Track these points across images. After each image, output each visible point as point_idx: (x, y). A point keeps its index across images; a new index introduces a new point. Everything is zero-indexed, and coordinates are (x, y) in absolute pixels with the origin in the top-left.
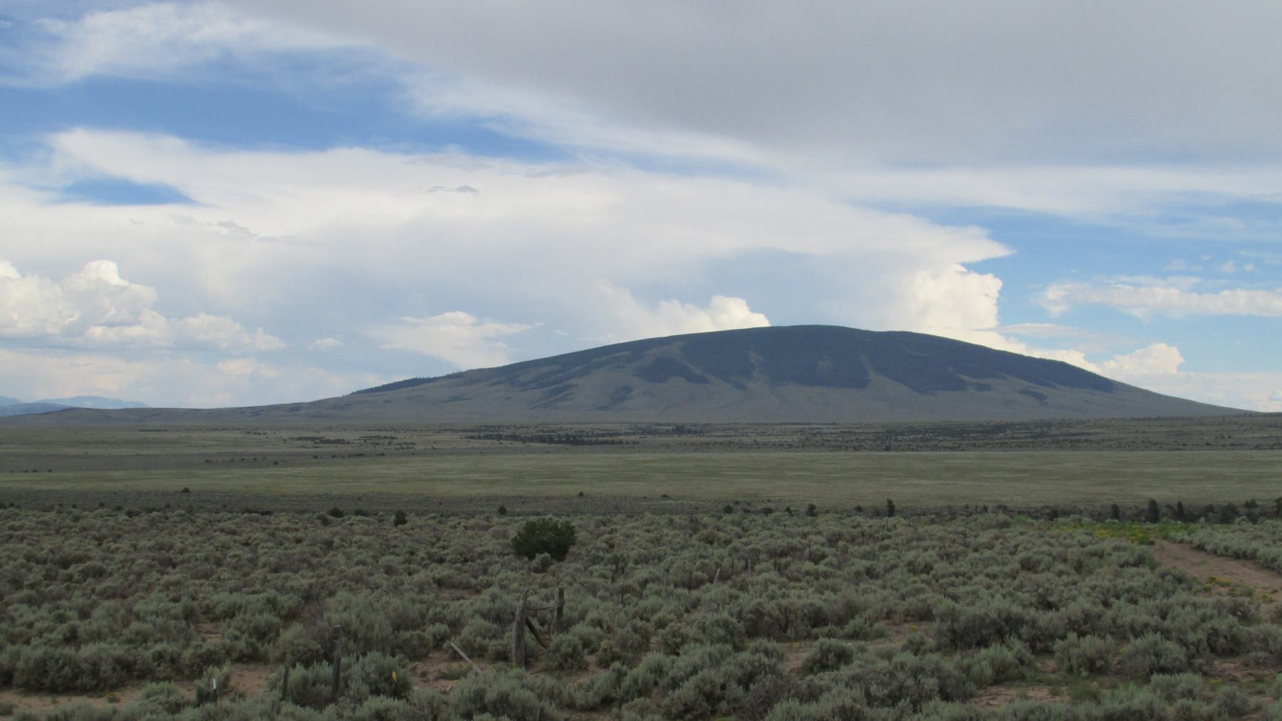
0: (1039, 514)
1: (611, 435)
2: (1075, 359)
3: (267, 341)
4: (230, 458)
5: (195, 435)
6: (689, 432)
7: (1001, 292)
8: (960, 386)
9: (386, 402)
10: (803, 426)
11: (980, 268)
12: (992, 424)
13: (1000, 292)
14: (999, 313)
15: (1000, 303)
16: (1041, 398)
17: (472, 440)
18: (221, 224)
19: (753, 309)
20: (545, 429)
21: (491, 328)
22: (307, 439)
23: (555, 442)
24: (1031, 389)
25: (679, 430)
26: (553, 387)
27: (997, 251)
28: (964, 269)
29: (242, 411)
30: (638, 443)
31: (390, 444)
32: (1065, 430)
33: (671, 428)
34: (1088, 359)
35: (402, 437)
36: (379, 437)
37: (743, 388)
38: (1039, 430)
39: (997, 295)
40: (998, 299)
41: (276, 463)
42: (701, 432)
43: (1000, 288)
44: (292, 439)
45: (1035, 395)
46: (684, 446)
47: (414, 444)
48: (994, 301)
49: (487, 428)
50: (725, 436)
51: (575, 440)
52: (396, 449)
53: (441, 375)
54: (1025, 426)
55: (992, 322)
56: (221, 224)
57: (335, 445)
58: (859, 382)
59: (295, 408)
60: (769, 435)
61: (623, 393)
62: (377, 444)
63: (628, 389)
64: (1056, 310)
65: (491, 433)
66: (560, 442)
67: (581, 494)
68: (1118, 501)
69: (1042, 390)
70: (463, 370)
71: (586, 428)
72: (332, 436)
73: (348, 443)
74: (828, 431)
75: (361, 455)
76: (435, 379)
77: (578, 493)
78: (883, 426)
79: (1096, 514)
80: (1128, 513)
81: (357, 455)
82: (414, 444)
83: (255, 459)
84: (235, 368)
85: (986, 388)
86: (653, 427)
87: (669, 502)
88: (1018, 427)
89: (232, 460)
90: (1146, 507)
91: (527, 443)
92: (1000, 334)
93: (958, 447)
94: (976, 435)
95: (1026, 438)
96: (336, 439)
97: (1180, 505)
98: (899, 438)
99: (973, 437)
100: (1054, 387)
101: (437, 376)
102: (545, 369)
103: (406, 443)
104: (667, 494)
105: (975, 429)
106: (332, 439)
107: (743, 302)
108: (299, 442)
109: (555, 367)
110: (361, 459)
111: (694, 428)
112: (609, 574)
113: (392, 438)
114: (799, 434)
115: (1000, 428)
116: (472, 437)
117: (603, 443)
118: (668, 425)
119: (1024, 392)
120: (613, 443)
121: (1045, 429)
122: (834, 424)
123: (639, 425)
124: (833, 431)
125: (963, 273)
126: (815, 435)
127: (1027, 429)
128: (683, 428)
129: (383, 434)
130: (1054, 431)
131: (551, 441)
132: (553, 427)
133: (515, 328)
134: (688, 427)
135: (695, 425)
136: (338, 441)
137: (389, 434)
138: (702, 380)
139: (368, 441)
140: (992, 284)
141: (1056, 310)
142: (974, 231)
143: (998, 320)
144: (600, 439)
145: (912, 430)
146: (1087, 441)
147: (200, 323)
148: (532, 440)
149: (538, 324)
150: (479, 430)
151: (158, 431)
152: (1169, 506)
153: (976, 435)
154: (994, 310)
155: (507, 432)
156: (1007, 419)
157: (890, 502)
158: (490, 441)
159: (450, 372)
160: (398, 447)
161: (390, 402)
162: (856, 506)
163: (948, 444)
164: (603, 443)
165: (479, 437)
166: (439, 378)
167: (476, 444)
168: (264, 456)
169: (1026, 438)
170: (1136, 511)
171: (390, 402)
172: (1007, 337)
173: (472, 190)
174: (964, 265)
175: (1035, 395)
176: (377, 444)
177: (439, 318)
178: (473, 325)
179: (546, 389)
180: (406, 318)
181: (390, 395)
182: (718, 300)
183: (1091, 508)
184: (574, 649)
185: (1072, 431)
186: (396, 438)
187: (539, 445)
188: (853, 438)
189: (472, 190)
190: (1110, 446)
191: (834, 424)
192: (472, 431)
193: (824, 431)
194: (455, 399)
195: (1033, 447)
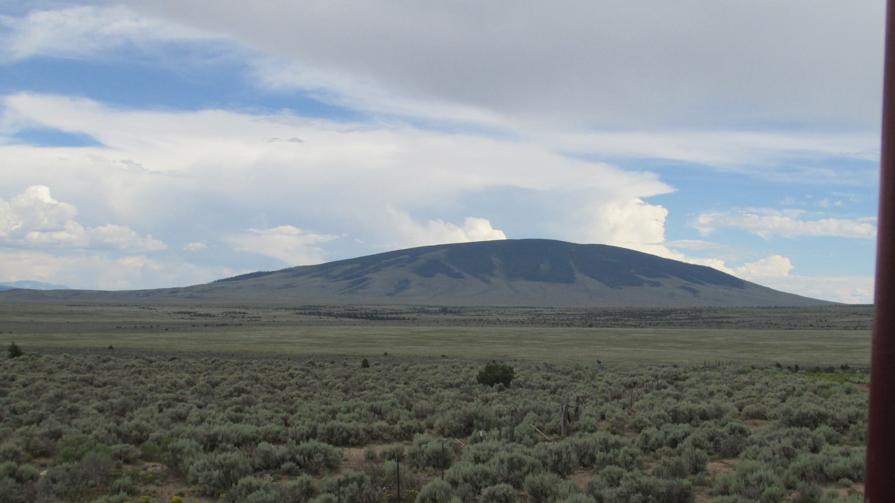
1: (397, 314)
2: (717, 265)
5: (105, 309)
6: (451, 312)
8: (639, 283)
11: (653, 201)
14: (666, 232)
15: (666, 225)
17: (301, 316)
18: (123, 161)
19: (495, 227)
21: (312, 237)
22: (185, 313)
24: (688, 286)
25: (444, 311)
26: (353, 280)
27: (664, 189)
28: (642, 202)
31: (243, 317)
32: (711, 315)
35: (250, 312)
37: (488, 282)
38: (694, 314)
39: (664, 220)
43: (666, 215)
44: (175, 313)
45: (690, 289)
46: (458, 323)
48: (662, 224)
49: (310, 307)
53: (277, 270)
54: (684, 311)
55: (660, 238)
56: (123, 161)
61: (403, 285)
63: (407, 281)
64: (705, 231)
65: (314, 311)
66: (362, 318)
69: (697, 287)
70: (292, 267)
73: (214, 316)
75: (225, 325)
76: (272, 273)
82: (260, 318)
84: (130, 262)
85: (657, 284)
89: (136, 327)
91: (339, 318)
95: (686, 319)
96: (204, 313)
99: (649, 318)
102: (349, 267)
104: (445, 354)
106: (202, 313)
107: (487, 222)
108: (180, 316)
111: (454, 310)
115: (667, 312)
119: (683, 287)
126: (539, 315)
129: (238, 310)
130: (704, 315)
131: (356, 317)
132: (356, 307)
133: (328, 238)
136: (207, 315)
138: (459, 276)
139: (228, 315)
140: (661, 212)
141: (705, 231)
143: (665, 237)
144: (390, 316)
145: (606, 313)
147: (108, 231)
149: (344, 235)
154: (662, 230)
161: (241, 288)
165: (305, 314)
168: (158, 325)
169: (686, 319)
172: (671, 249)
173: (300, 141)
174: (641, 198)
175: (690, 289)
177: (275, 230)
180: (251, 230)
182: (470, 220)
185: (716, 315)
189: (300, 141)
191: (552, 308)
194: (286, 286)
195: (691, 326)
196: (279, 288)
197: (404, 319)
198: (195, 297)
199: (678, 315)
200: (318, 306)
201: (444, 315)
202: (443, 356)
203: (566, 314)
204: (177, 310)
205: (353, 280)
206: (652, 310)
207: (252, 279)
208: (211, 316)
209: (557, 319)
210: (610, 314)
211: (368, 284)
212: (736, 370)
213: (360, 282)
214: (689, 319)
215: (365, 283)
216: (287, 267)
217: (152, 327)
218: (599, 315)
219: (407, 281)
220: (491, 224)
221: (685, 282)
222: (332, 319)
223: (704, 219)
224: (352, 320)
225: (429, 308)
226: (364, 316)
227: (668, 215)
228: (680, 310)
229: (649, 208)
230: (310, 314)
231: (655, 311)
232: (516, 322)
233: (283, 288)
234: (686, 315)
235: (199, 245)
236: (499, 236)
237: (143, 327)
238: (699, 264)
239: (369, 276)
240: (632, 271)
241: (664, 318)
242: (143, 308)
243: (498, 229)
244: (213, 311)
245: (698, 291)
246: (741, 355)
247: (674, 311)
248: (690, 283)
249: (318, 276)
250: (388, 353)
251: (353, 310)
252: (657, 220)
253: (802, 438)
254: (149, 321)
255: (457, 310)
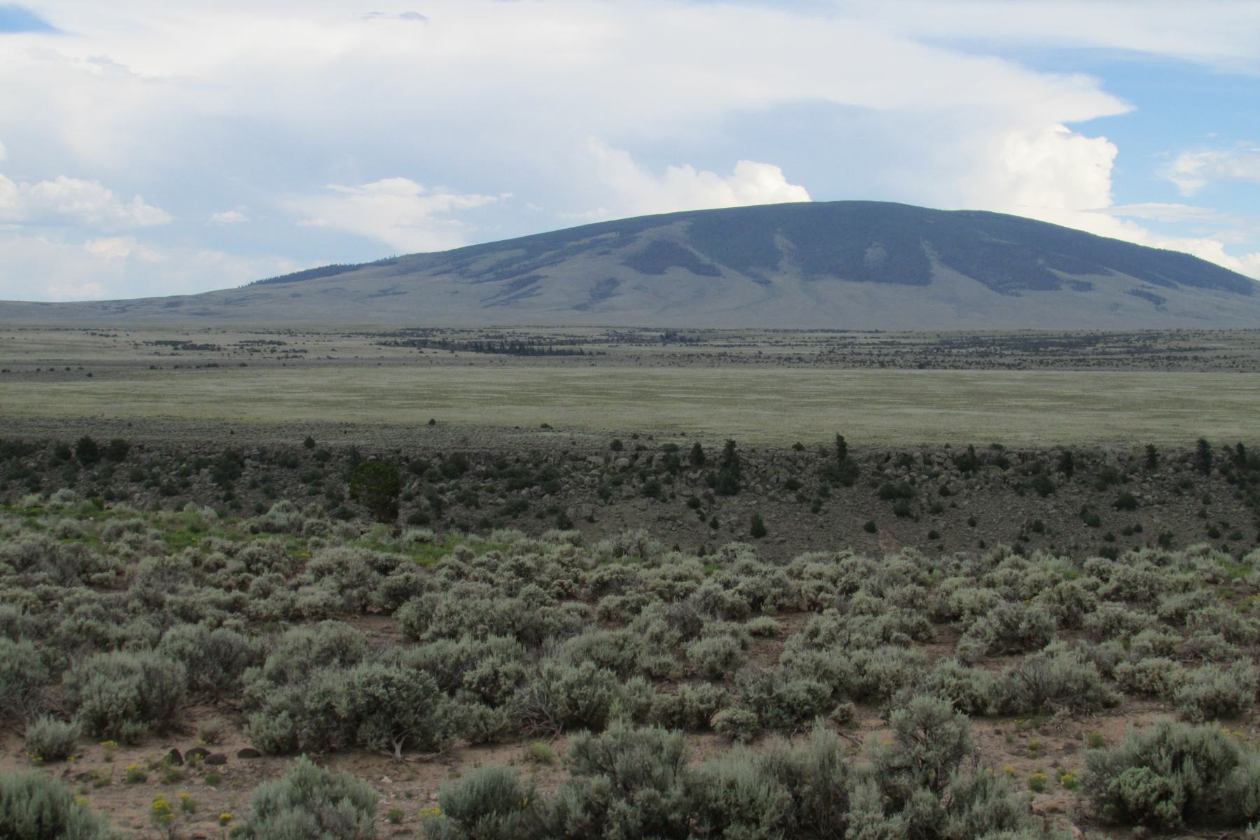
0: (1046, 457)
1: (573, 343)
2: (1209, 251)
3: (144, 213)
4: (36, 367)
5: (20, 337)
6: (683, 340)
7: (1116, 161)
8: (1051, 284)
9: (294, 296)
10: (830, 334)
11: (1089, 129)
12: (1083, 335)
13: (1114, 161)
14: (1113, 189)
15: (1114, 176)
16: (1157, 301)
17: (383, 347)
18: (93, 60)
19: (791, 179)
20: (491, 335)
21: (443, 200)
22: (166, 343)
23: (495, 351)
24: (1145, 290)
25: (670, 337)
26: (511, 280)
27: (1112, 106)
28: (1067, 130)
29: (103, 306)
30: (604, 354)
31: (273, 351)
32: (1173, 344)
33: (658, 334)
34: (1228, 250)
35: (292, 342)
36: (263, 342)
37: (766, 283)
38: (1140, 344)
39: (1111, 165)
40: (1112, 171)
41: (90, 375)
42: (698, 340)
43: (1114, 157)
44: (147, 343)
45: (1149, 297)
46: (674, 360)
47: (305, 351)
48: (1108, 173)
49: (415, 331)
50: (725, 346)
51: (521, 349)
52: (279, 358)
53: (369, 261)
54: (1126, 338)
55: (1103, 200)
56: (93, 60)
57: (200, 352)
58: (921, 277)
59: (174, 303)
60: (784, 346)
61: (605, 289)
62: (256, 351)
63: (613, 282)
64: (1187, 187)
65: (418, 339)
66: (503, 351)
67: (432, 422)
68: (1159, 441)
69: (1160, 291)
70: (397, 256)
71: (545, 333)
72: (199, 340)
73: (219, 349)
74: (865, 341)
75: (215, 365)
76: (359, 267)
77: (427, 420)
78: (938, 336)
79: (1126, 458)
80: (1170, 457)
81: (209, 366)
82: (305, 351)
83: (81, 369)
84: (106, 248)
85: (1088, 287)
86: (637, 333)
87: (548, 434)
88: (1115, 338)
89: (38, 370)
90: (1194, 449)
91: (457, 352)
92: (1114, 216)
93: (1019, 364)
94: (1055, 349)
95: (1121, 353)
96: (203, 343)
97: (1240, 447)
98: (954, 351)
99: (1052, 351)
100: (1176, 287)
101: (363, 262)
102: (504, 255)
103: (294, 351)
104: (549, 424)
105: (1058, 341)
106: (198, 344)
107: (777, 170)
108: (155, 348)
109: (520, 252)
110: (211, 370)
111: (689, 336)
112: (1089, 510)
113: (279, 343)
114: (824, 344)
115: (1092, 340)
116: (385, 344)
117: (558, 353)
118: (656, 330)
119: (1136, 293)
120: (571, 353)
121: (1148, 343)
122: (877, 331)
123: (619, 331)
124: (870, 341)
125: (1066, 136)
126: (845, 346)
127: (1126, 341)
128: (675, 334)
129: (268, 338)
130: (1160, 345)
131: (490, 349)
132: (503, 332)
133: (474, 201)
134: (682, 334)
135: (693, 332)
136: (205, 347)
137: (275, 338)
138: (711, 271)
139: (246, 347)
140: (1104, 150)
141: (1187, 187)
142: (1081, 80)
143: (1112, 199)
144: (555, 348)
145: (976, 341)
146: (1196, 358)
147: (58, 188)
148: (465, 348)
149: (506, 195)
150: (402, 335)
151: (57, 329)
152: (1226, 448)
153: (1055, 349)
154: (1107, 185)
155: (439, 338)
156: (1105, 329)
157: (840, 439)
158: (408, 349)
159: (381, 256)
160: (283, 355)
161: (299, 296)
162: (795, 442)
163: (1007, 360)
164: (558, 353)
165: (396, 344)
166: (366, 265)
167: (388, 353)
168: (81, 366)
169: (1121, 353)
170: (1179, 455)
171: (299, 296)
172: (1123, 219)
173: (422, 18)
174: (1067, 125)
175: (1149, 297)
176: (256, 351)
177: (373, 186)
178: (419, 195)
179: (504, 281)
180: (330, 186)
181: (300, 286)
182: (744, 166)
183: (1119, 450)
184: (961, 610)
185: (1183, 345)
186: (285, 344)
187: (473, 354)
188: (892, 351)
189: (422, 18)
190: (1219, 366)
191: (877, 331)
192: (394, 335)
193: (857, 341)
194: (384, 293)
195: (1117, 366)
196: (370, 296)
197: (582, 353)
198: (211, 314)
199: (1110, 345)
200: (432, 330)
201: (664, 345)
202: (545, 426)
203: (900, 344)
204: (154, 338)
205: (511, 280)
206: (1067, 336)
207: (317, 280)
208: (213, 350)
209: (875, 352)
210: (981, 344)
211: (540, 287)
212: (119, 515)
213: (523, 284)
214: (1128, 352)
215: (533, 286)
216: (386, 255)
217: (68, 369)
218: (960, 346)
219: (613, 282)
220: (784, 173)
221: (1140, 282)
222: (444, 354)
223: (1186, 163)
224: (481, 355)
225: (642, 333)
226: (507, 348)
227: (1117, 156)
228: (1117, 336)
229: (1081, 144)
230: (405, 344)
231: (1070, 337)
232: (789, 359)
233: (378, 295)
234: (1126, 344)
235: (230, 216)
236: (798, 195)
237: (52, 370)
238: (1182, 250)
239: (540, 272)
240: (1040, 262)
241: (1080, 351)
242: (93, 334)
243: (796, 184)
244: (220, 340)
245: (1165, 300)
246: (1150, 424)
247: (1105, 338)
248: (1150, 285)
249: (446, 272)
250: (437, 420)
251: (495, 337)
252: (1097, 165)
253: (808, 781)
254: (66, 358)
255: (694, 336)
